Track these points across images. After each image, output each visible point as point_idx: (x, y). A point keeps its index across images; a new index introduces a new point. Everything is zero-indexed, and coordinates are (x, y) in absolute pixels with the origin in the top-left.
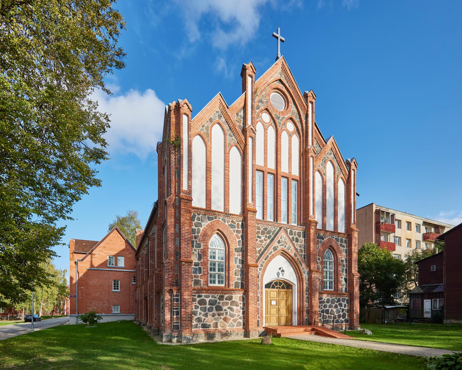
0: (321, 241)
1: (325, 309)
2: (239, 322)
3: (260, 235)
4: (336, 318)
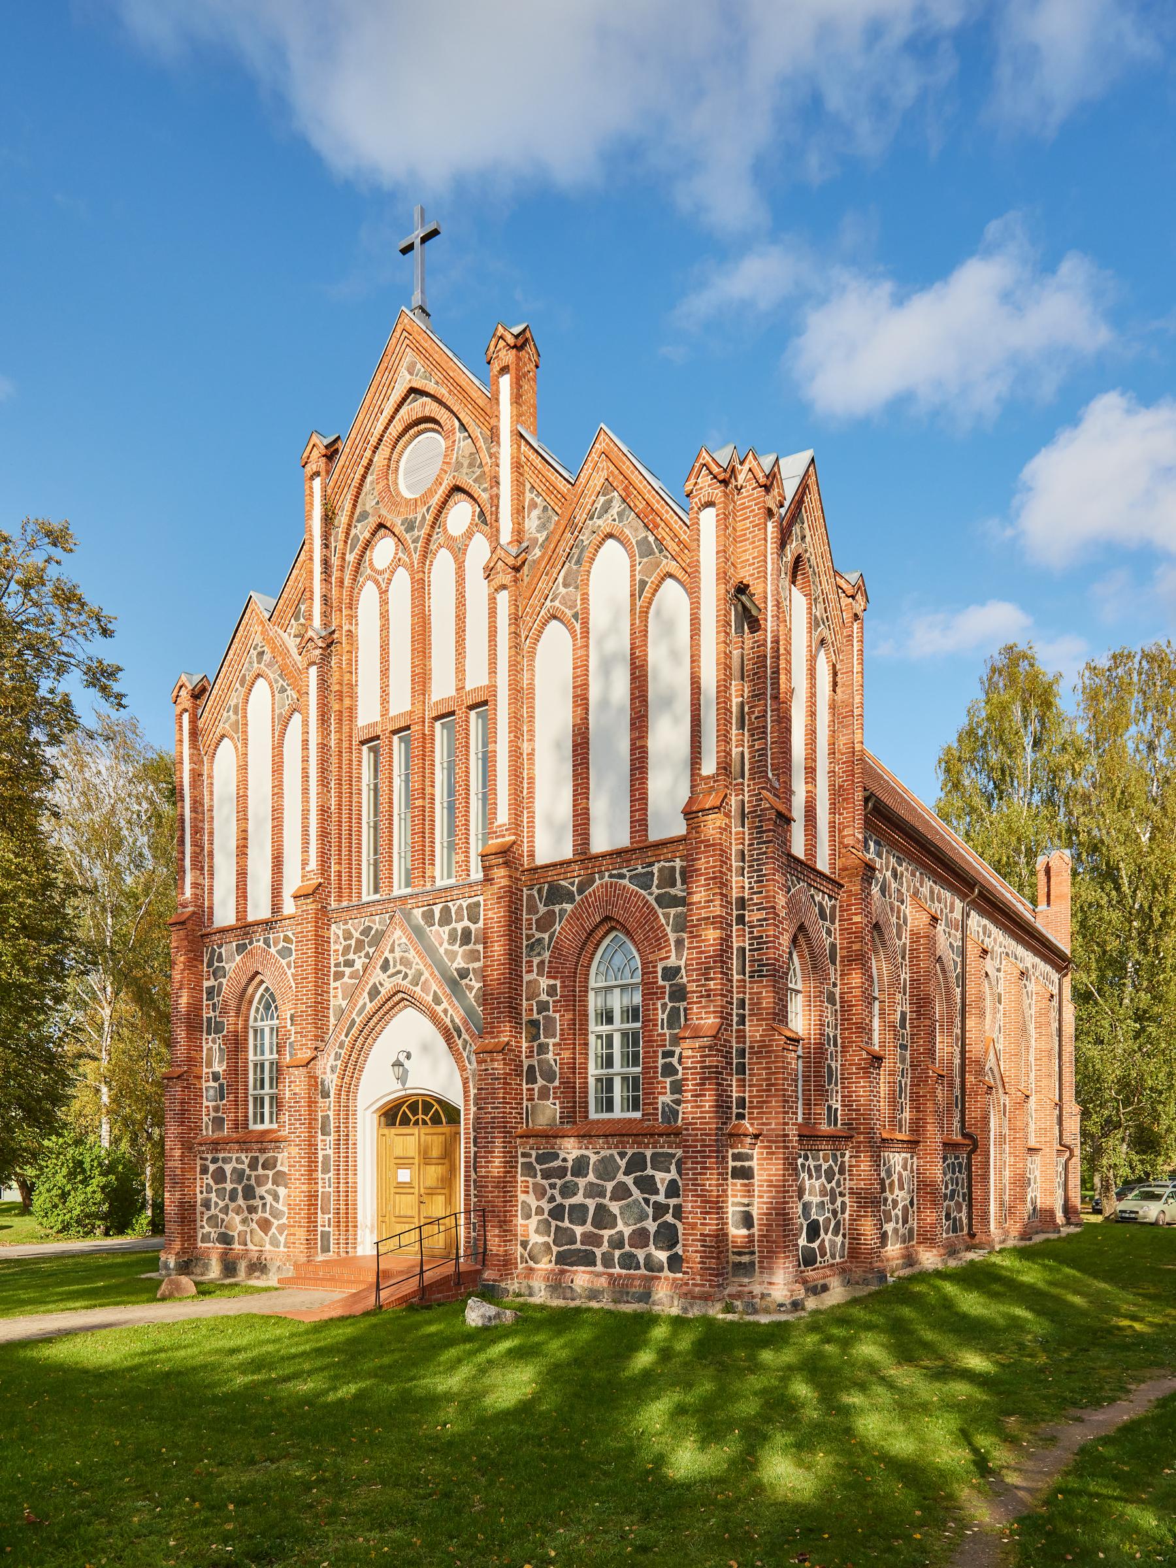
1: (568, 1202)
3: (351, 956)
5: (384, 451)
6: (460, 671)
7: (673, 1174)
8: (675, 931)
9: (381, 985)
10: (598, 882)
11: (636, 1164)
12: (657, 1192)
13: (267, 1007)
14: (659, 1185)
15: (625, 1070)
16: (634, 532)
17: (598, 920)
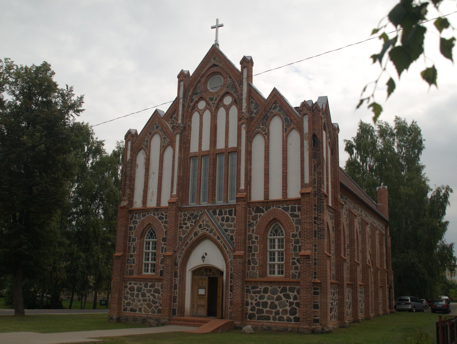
0: (260, 215)
2: (159, 309)
3: (186, 222)
4: (279, 314)
5: (204, 78)
7: (295, 293)
8: (296, 224)
9: (199, 232)
10: (272, 208)
11: (284, 290)
12: (290, 298)
13: (151, 234)
14: (291, 296)
15: (279, 262)
17: (272, 219)
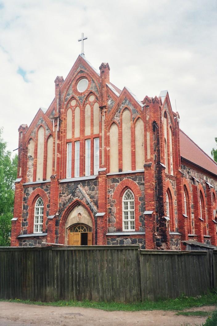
6: (73, 133)
16: (131, 108)
